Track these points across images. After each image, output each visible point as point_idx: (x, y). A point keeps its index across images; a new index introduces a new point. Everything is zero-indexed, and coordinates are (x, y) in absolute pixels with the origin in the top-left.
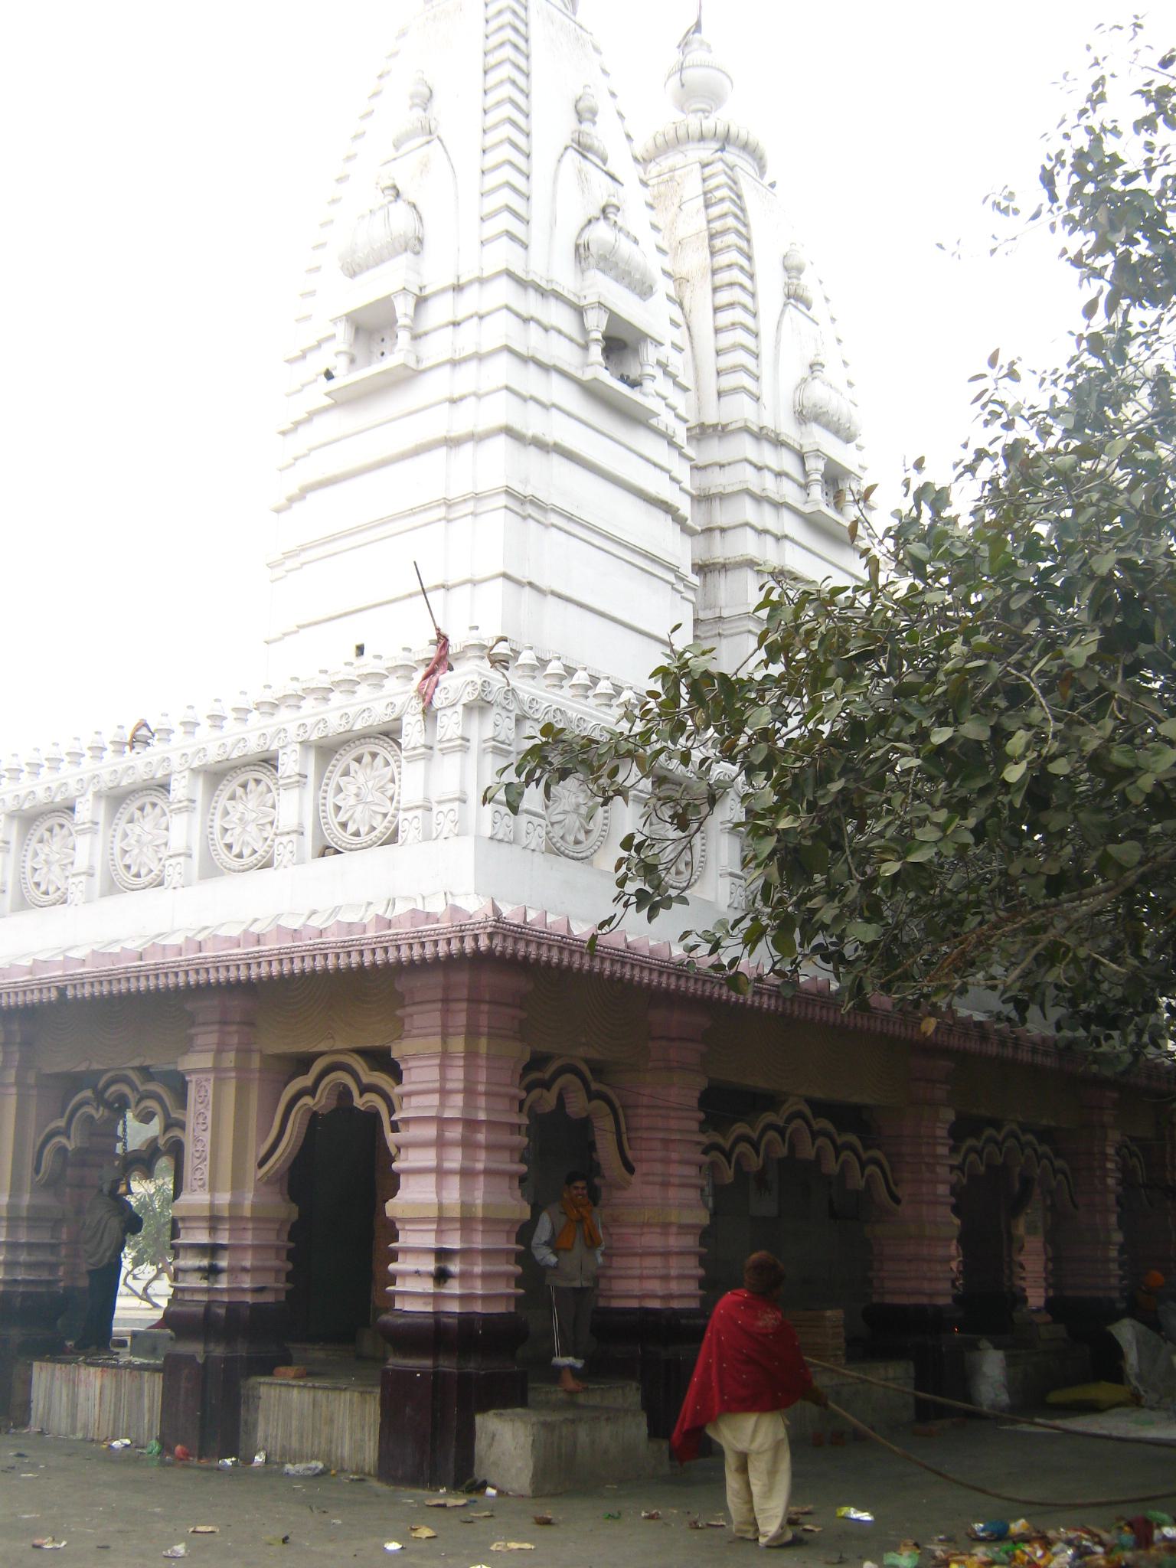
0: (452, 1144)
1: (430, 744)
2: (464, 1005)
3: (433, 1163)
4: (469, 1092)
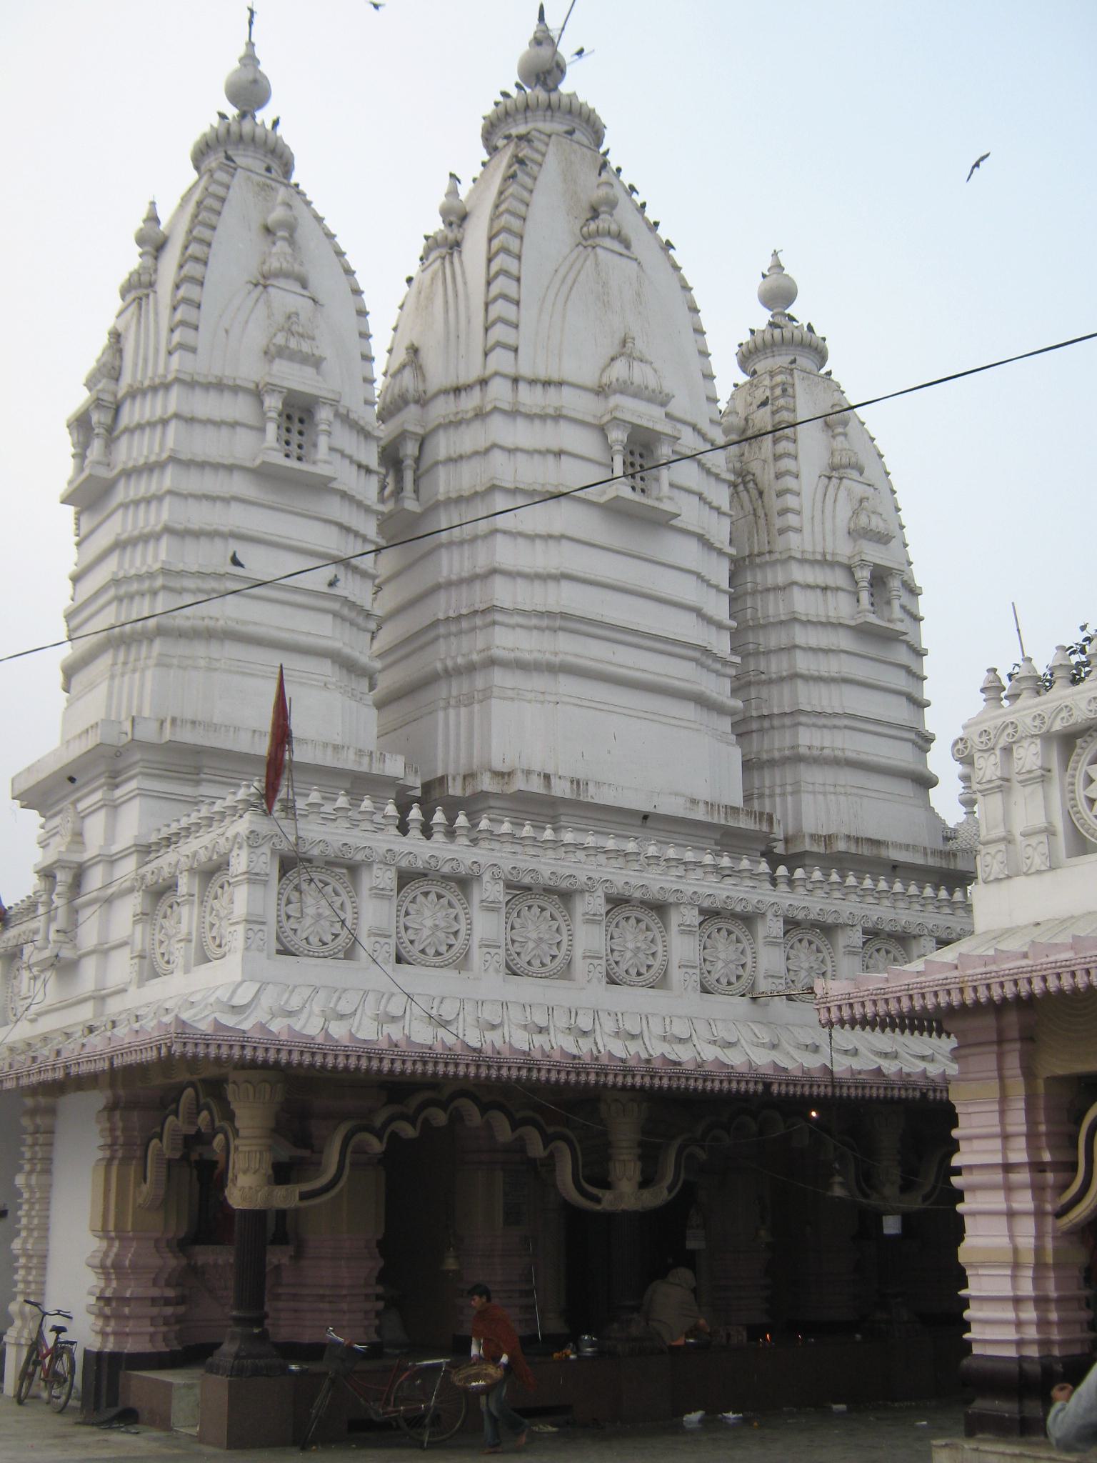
0: (1021, 1187)
1: (1006, 776)
2: (1017, 1046)
3: (1003, 1206)
4: (1031, 1136)
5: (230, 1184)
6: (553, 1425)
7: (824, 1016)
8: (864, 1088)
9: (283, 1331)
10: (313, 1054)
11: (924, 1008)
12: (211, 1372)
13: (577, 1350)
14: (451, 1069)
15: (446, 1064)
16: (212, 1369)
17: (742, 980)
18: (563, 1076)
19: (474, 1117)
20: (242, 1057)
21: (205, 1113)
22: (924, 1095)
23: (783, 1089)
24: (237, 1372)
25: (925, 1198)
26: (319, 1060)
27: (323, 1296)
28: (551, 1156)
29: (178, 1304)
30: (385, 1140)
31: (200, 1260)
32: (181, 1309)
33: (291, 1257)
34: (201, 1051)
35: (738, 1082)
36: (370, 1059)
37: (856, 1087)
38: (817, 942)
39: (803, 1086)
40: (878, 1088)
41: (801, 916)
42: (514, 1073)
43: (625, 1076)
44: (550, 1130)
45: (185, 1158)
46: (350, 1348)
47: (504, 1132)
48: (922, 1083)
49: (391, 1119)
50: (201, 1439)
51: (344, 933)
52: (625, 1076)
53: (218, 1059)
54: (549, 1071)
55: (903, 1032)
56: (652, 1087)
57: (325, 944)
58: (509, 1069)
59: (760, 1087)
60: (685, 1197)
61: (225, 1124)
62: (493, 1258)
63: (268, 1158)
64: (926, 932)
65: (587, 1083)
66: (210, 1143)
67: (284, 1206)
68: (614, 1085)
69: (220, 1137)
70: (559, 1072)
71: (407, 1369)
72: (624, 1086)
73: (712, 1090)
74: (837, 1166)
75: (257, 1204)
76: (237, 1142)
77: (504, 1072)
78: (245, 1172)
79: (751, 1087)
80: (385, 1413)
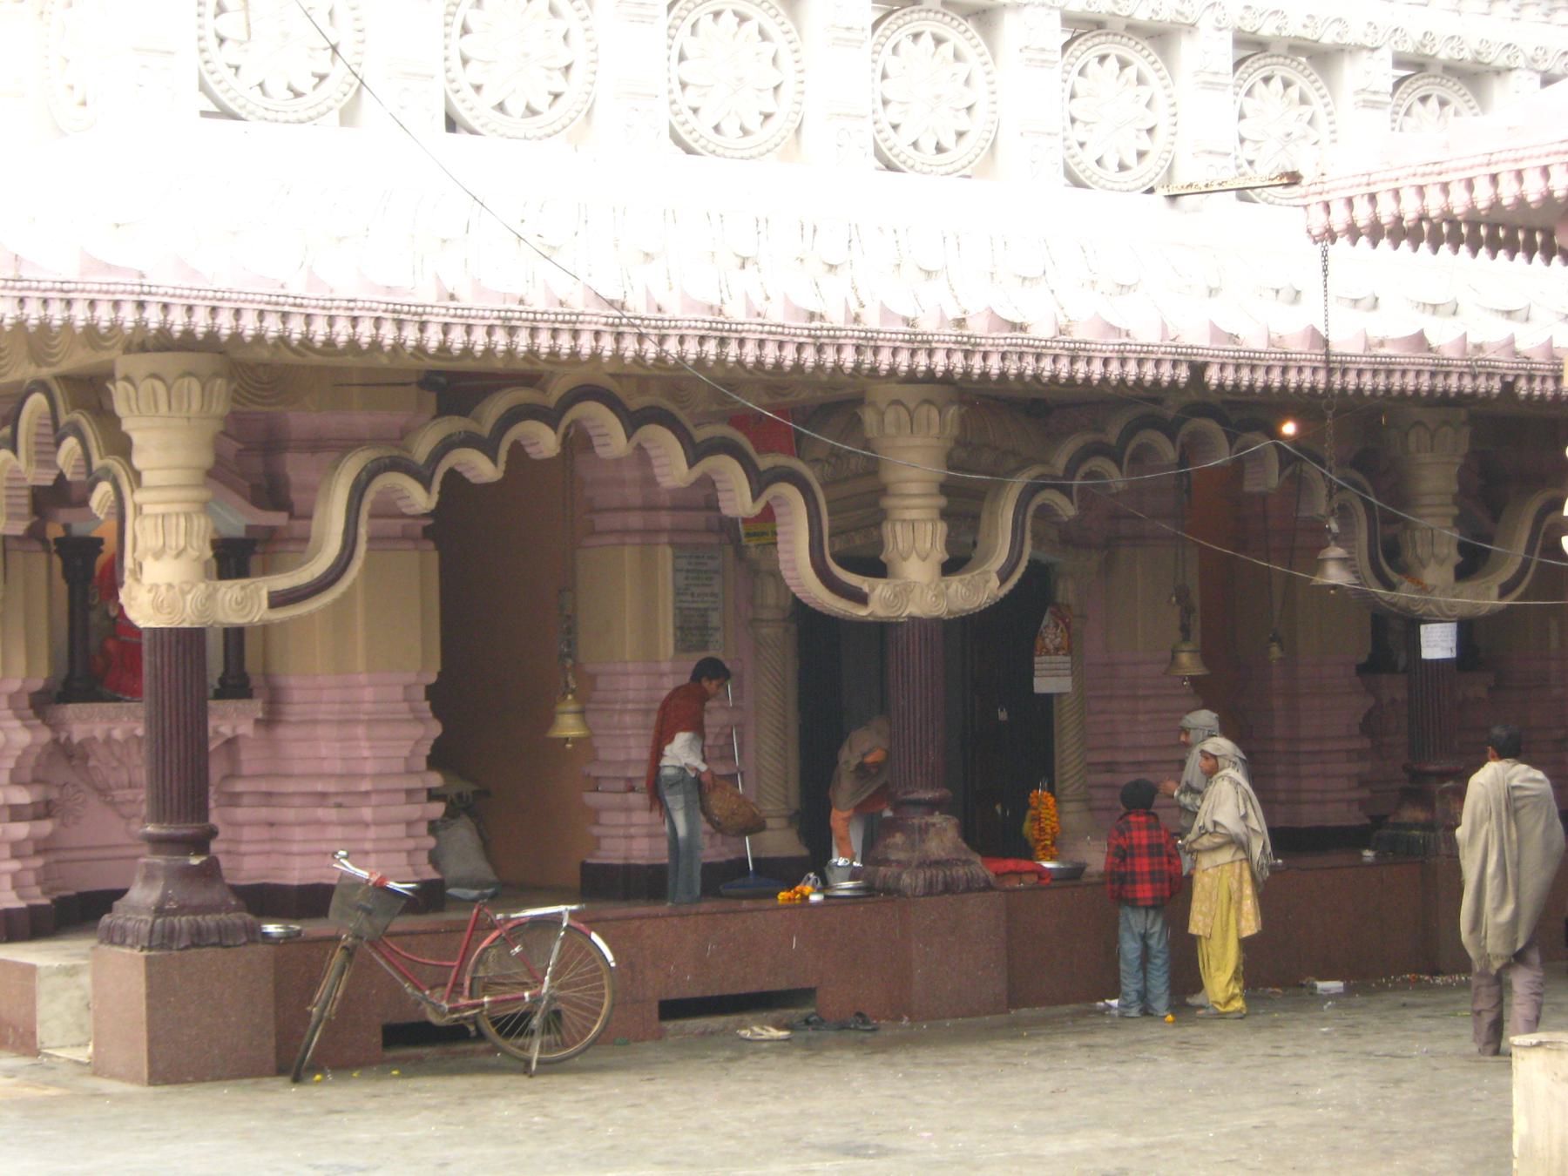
5: (128, 579)
6: (778, 1027)
7: (1318, 221)
8: (1389, 373)
9: (250, 863)
10: (285, 316)
11: (1521, 201)
12: (112, 943)
13: (824, 885)
14: (565, 343)
15: (555, 332)
16: (114, 937)
17: (1148, 160)
18: (789, 355)
19: (612, 438)
20: (141, 326)
21: (71, 443)
22: (1508, 387)
23: (1229, 375)
24: (161, 940)
25: (1505, 591)
26: (296, 328)
27: (324, 795)
28: (768, 514)
29: (37, 817)
30: (436, 486)
31: (78, 732)
32: (46, 827)
33: (257, 721)
34: (57, 314)
35: (1140, 362)
36: (400, 324)
37: (1375, 373)
38: (1301, 83)
39: (1269, 369)
40: (1418, 373)
41: (1267, 30)
42: (691, 349)
43: (913, 353)
44: (766, 462)
45: (35, 534)
46: (380, 887)
47: (673, 467)
48: (1504, 361)
49: (445, 447)
50: (97, 1068)
51: (338, 72)
52: (913, 353)
53: (91, 329)
54: (761, 343)
55: (1475, 252)
56: (967, 373)
57: (298, 95)
58: (682, 340)
59: (1183, 373)
60: (1031, 597)
61: (114, 463)
62: (640, 751)
63: (202, 527)
64: (1521, 62)
65: (838, 368)
66: (84, 502)
67: (236, 620)
68: (893, 371)
69: (104, 489)
70: (781, 345)
71: (493, 926)
72: (912, 372)
73: (1088, 379)
74: (1334, 526)
75: (185, 616)
76: (140, 496)
77: (672, 347)
78: (158, 555)
79: (1166, 372)
80: (453, 1010)
